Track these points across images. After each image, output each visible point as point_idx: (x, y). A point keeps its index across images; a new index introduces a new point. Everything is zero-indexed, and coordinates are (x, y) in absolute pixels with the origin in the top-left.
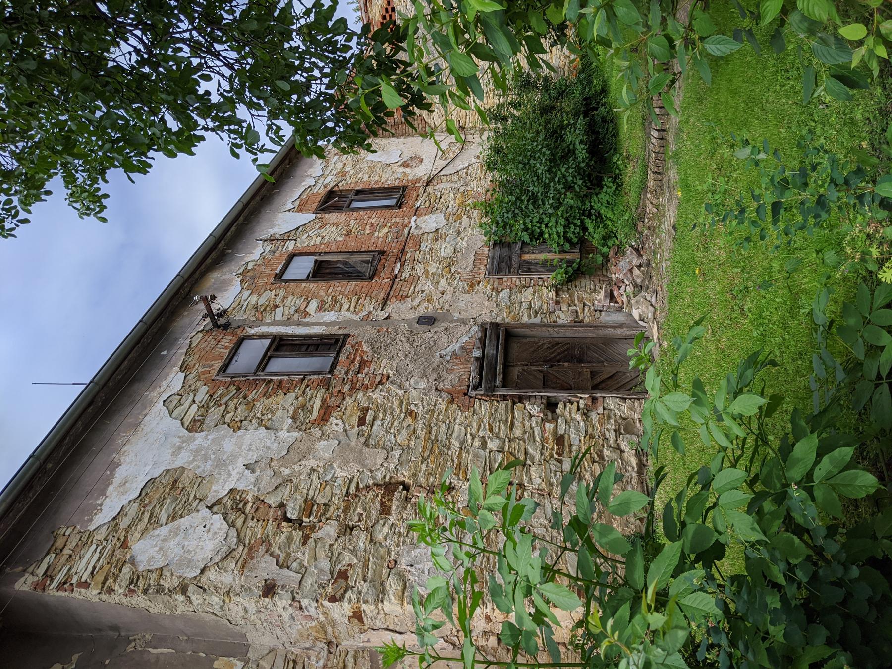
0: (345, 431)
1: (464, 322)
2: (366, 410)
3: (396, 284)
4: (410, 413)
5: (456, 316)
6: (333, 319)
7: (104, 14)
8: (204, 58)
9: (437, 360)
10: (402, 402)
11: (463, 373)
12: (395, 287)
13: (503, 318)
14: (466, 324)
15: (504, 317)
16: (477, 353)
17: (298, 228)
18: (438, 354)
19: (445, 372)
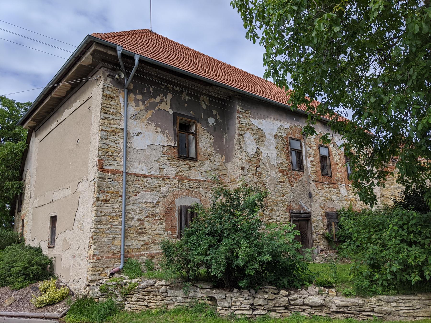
1: (311, 206)
2: (284, 182)
4: (284, 195)
5: (312, 204)
6: (308, 166)
11: (296, 208)
15: (313, 218)
16: (302, 212)
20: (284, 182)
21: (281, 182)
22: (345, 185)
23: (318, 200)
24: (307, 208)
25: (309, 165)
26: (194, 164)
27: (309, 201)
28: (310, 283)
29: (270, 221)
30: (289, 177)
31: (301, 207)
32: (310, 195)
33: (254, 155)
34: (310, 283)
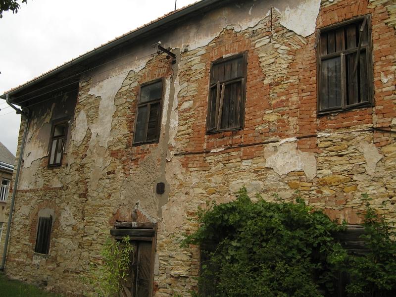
0: (106, 167)
1: (159, 213)
2: (114, 173)
3: (200, 155)
4: (110, 196)
5: (164, 207)
6: (172, 126)
7: (39, 133)
8: (148, 76)
9: (135, 202)
10: (115, 189)
11: (126, 215)
12: (198, 155)
13: (161, 239)
14: (158, 215)
15: (161, 237)
16: (134, 224)
17: (291, 31)
18: (138, 201)
19: (128, 207)
20: (114, 173)
21: (109, 173)
22: (294, 139)
23: (183, 197)
24: (149, 216)
25: (174, 122)
26: (59, 170)
27: (158, 201)
28: (47, 189)
29: (84, 239)
30: (124, 161)
31: (136, 215)
32: (161, 189)
33: (83, 141)
34: (47, 189)
